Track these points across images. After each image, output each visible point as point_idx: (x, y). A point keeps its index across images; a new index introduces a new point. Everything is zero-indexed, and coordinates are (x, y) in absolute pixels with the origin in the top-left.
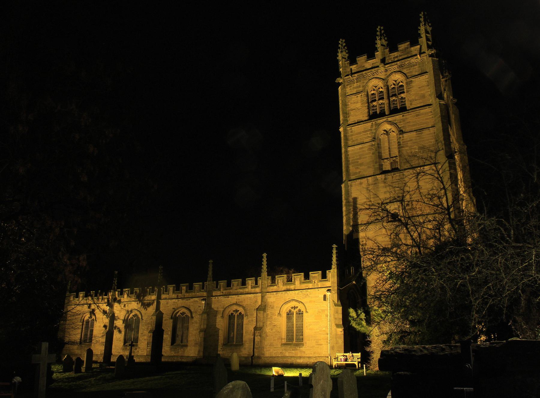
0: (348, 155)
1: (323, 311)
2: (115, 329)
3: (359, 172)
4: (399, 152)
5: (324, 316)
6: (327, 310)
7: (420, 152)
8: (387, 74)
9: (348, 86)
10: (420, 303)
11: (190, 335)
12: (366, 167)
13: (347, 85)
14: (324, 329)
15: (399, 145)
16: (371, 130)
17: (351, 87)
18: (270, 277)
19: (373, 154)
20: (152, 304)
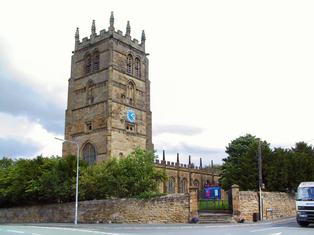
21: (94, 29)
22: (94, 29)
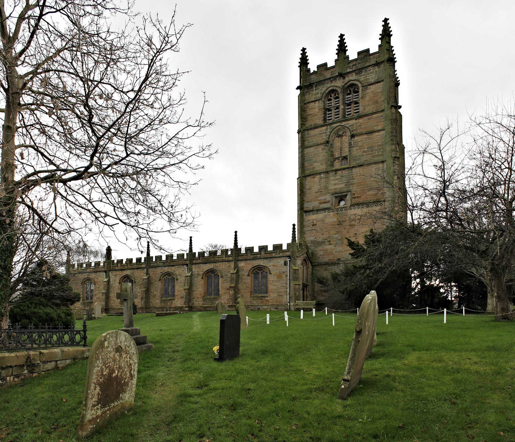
0: (304, 154)
1: (284, 272)
2: (139, 334)
3: (313, 168)
4: (350, 151)
5: (285, 275)
6: (287, 271)
7: (369, 151)
8: (344, 82)
9: (308, 93)
10: (425, 266)
11: (176, 291)
12: (319, 164)
13: (307, 92)
14: (284, 285)
15: (350, 145)
16: (326, 133)
17: (310, 94)
18: (239, 247)
19: (326, 152)
20: (307, 282)
21: (342, 48)
22: (342, 48)
